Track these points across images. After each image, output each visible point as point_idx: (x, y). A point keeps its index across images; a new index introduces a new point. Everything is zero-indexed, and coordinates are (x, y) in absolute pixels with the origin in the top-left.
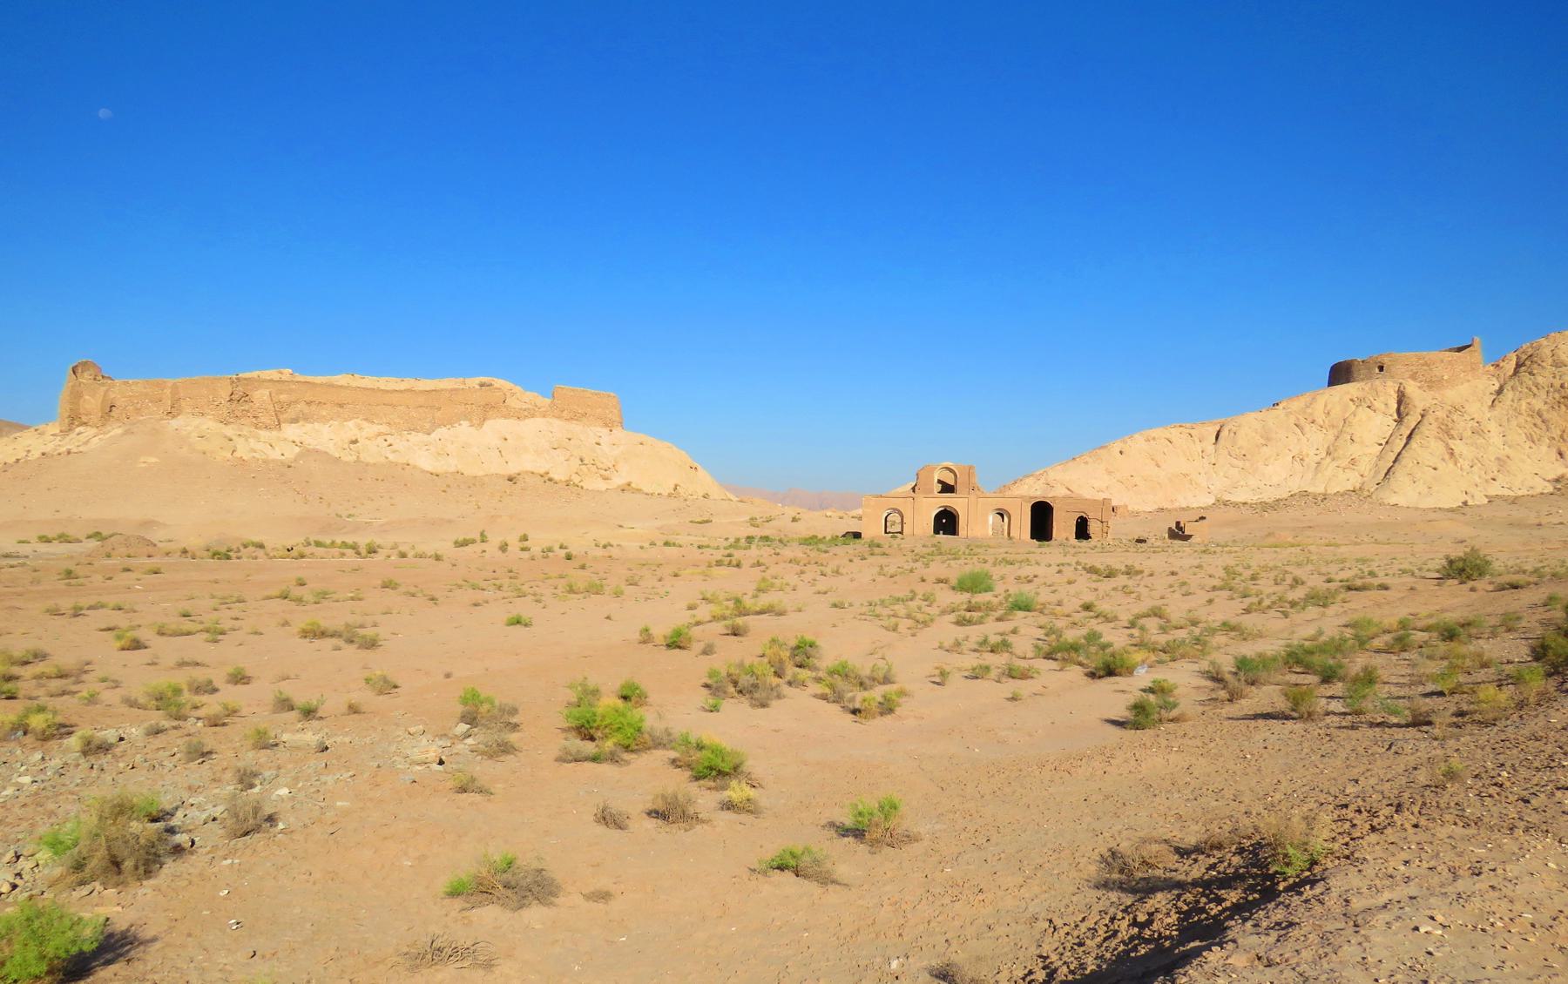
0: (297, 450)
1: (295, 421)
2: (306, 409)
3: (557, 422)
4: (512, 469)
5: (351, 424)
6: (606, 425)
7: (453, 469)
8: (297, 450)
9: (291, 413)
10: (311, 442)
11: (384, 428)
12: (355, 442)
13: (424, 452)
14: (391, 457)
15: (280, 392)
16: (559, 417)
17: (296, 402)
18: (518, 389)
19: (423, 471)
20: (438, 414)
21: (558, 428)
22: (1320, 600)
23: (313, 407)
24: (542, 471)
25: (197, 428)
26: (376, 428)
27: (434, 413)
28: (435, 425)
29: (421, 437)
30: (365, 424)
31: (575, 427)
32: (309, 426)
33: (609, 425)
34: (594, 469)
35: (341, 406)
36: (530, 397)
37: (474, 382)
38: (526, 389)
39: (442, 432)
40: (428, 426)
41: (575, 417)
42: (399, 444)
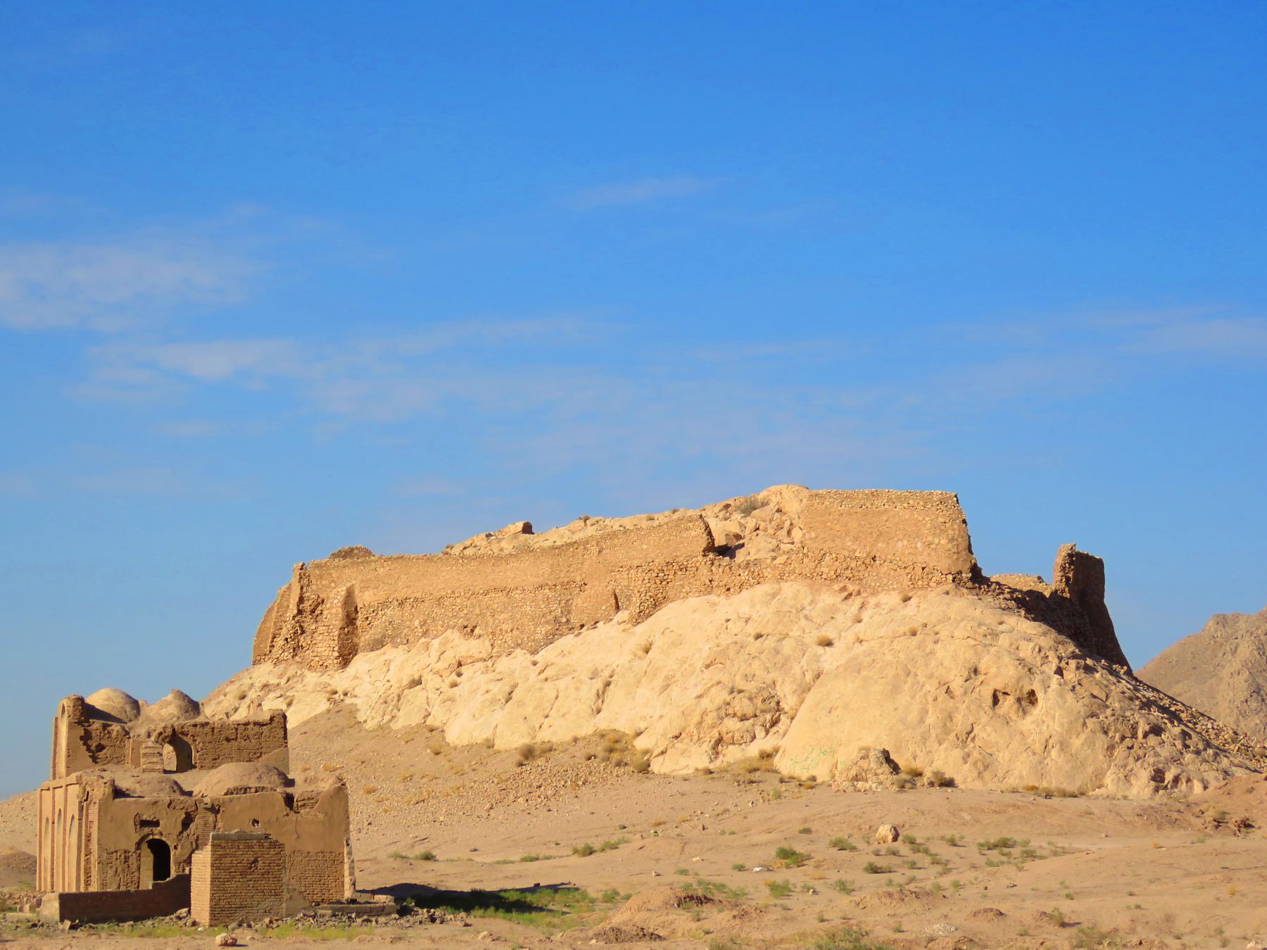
1: (378, 644)
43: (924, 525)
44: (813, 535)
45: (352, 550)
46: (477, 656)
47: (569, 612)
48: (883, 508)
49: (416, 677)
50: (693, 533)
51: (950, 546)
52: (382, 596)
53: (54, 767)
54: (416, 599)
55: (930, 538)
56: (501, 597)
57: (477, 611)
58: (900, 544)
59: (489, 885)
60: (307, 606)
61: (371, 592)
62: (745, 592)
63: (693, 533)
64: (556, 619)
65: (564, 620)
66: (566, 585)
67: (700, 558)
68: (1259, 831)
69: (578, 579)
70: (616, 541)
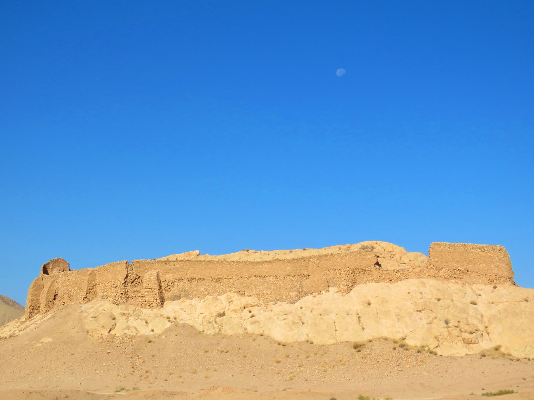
0: (168, 325)
1: (177, 298)
2: (187, 286)
3: (431, 282)
4: (362, 337)
5: (222, 298)
6: (491, 281)
7: (303, 339)
8: (168, 325)
9: (175, 291)
10: (185, 318)
11: (252, 300)
12: (222, 315)
13: (278, 323)
14: (250, 329)
15: (167, 272)
16: (435, 277)
17: (179, 280)
18: (398, 249)
19: (273, 341)
20: (306, 282)
21: (431, 287)
22: (210, 262)
23: (194, 284)
24: (398, 337)
25: (100, 314)
26: (244, 300)
27: (300, 283)
28: (301, 294)
29: (286, 306)
30: (236, 297)
31: (453, 286)
32: (188, 302)
33: (494, 281)
34: (455, 332)
35: (217, 280)
36: (417, 258)
37: (356, 247)
38: (409, 249)
39: (308, 300)
40: (293, 294)
41: (456, 275)
42: (260, 314)
43: (495, 258)
44: (436, 260)
45: (58, 259)
46: (253, 304)
47: (302, 287)
48: (470, 251)
49: (221, 312)
50: (369, 257)
51: (506, 267)
52: (177, 277)
53: (495, 395)
54: (200, 279)
55: (498, 264)
56: (260, 280)
57: (474, 280)
58: (481, 265)
59: (503, 389)
60: (129, 279)
61: (171, 275)
62: (399, 282)
63: (369, 257)
64: (298, 289)
65: (301, 290)
66: (300, 275)
67: (372, 267)
68: (310, 335)
69: (306, 273)
70: (327, 258)
